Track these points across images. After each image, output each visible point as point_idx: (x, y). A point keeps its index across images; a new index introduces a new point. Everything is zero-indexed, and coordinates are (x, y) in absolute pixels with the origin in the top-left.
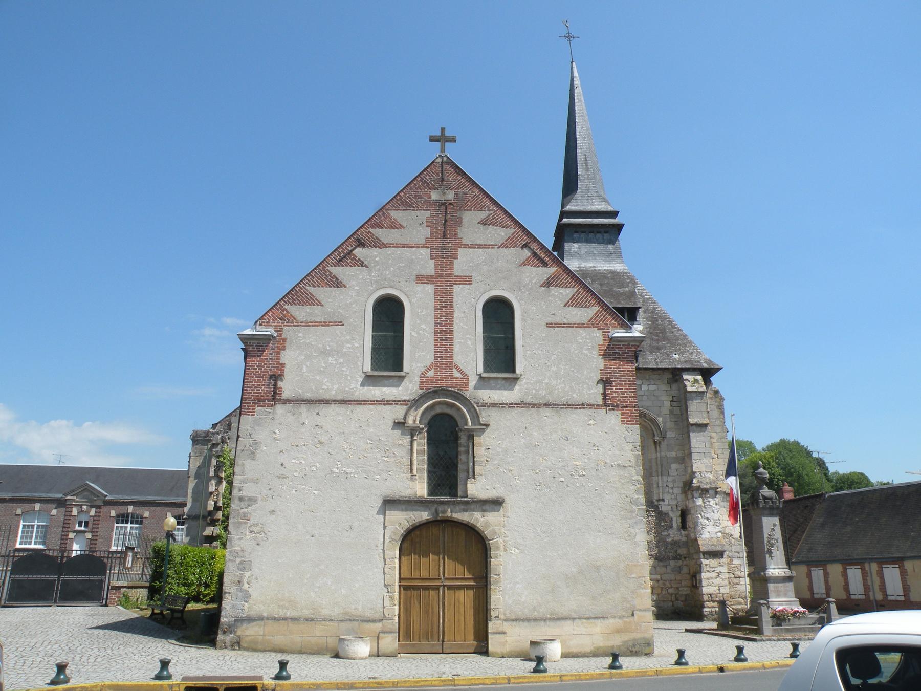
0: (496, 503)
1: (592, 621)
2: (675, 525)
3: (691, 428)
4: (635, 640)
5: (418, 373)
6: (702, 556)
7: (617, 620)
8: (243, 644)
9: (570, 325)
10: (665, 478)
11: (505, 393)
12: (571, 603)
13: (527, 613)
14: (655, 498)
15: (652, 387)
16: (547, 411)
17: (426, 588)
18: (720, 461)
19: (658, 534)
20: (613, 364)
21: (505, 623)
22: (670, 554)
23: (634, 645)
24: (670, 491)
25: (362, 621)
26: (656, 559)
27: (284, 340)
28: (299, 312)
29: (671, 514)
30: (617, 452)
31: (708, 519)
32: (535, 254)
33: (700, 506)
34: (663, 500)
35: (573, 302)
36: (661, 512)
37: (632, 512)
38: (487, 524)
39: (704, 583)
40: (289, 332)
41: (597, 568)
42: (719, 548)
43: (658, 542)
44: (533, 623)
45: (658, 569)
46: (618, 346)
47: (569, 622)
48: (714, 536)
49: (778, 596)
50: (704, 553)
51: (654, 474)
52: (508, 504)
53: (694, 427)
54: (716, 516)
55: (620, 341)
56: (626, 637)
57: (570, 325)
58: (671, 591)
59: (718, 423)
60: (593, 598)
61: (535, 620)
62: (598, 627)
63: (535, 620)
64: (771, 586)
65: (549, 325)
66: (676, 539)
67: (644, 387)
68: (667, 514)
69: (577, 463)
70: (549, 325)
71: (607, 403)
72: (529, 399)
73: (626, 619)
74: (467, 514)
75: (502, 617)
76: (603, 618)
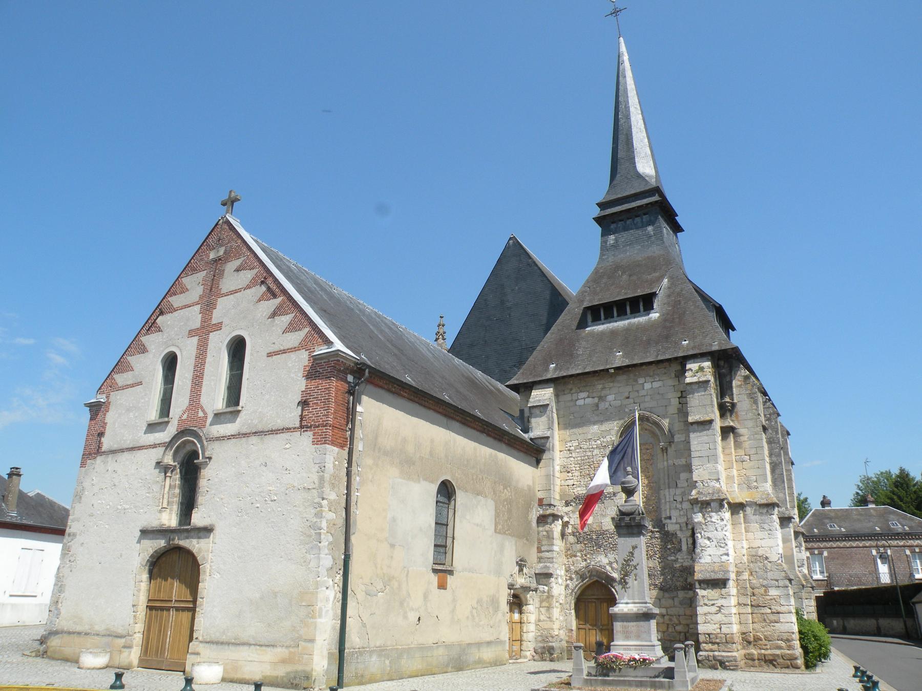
0: (207, 531)
1: (264, 648)
2: (684, 547)
3: (691, 428)
4: (296, 672)
5: (177, 417)
6: (697, 586)
7: (284, 649)
8: (49, 654)
9: (284, 352)
10: (672, 491)
11: (229, 425)
12: (252, 629)
13: (214, 637)
14: (664, 516)
15: (656, 385)
16: (254, 439)
17: (162, 609)
18: (752, 464)
19: (663, 558)
20: (314, 383)
21: (201, 645)
22: (678, 584)
23: (295, 678)
24: (679, 506)
25: (116, 637)
26: (661, 589)
27: (109, 403)
28: (120, 379)
29: (679, 534)
30: (305, 475)
31: (709, 539)
32: (269, 289)
33: (700, 523)
34: (670, 518)
35: (291, 328)
36: (668, 532)
37: (310, 536)
38: (200, 550)
39: (700, 619)
40: (116, 397)
41: (275, 594)
42: (720, 576)
43: (663, 568)
44: (220, 647)
45: (663, 601)
46: (319, 365)
47: (246, 648)
48: (716, 560)
49: (627, 638)
50: (701, 582)
51: (662, 487)
52: (217, 531)
53: (695, 426)
54: (720, 535)
55: (322, 359)
56: (289, 668)
57: (284, 352)
58: (679, 628)
59: (750, 415)
60: (269, 625)
61: (222, 643)
62: (269, 655)
63: (222, 643)
64: (618, 626)
65: (270, 355)
66: (685, 564)
67: (647, 386)
68: (674, 535)
69: (271, 488)
70: (270, 355)
71: (303, 427)
72: (244, 430)
73: (291, 649)
74: (188, 541)
75: (200, 638)
76: (273, 646)
